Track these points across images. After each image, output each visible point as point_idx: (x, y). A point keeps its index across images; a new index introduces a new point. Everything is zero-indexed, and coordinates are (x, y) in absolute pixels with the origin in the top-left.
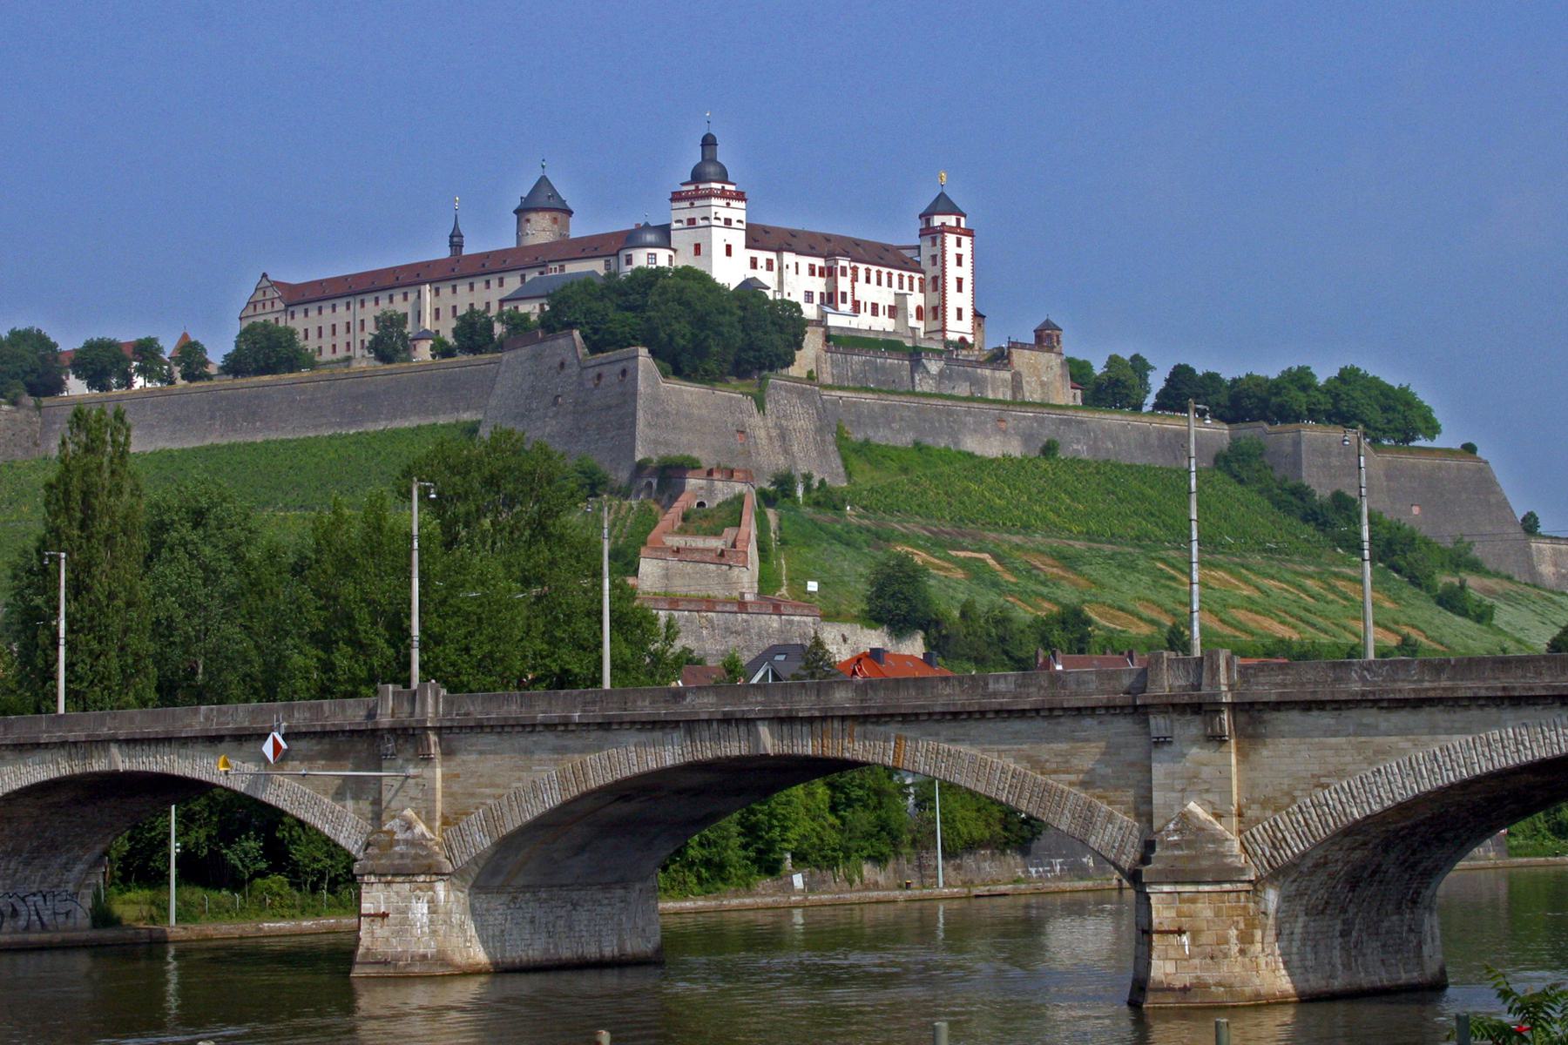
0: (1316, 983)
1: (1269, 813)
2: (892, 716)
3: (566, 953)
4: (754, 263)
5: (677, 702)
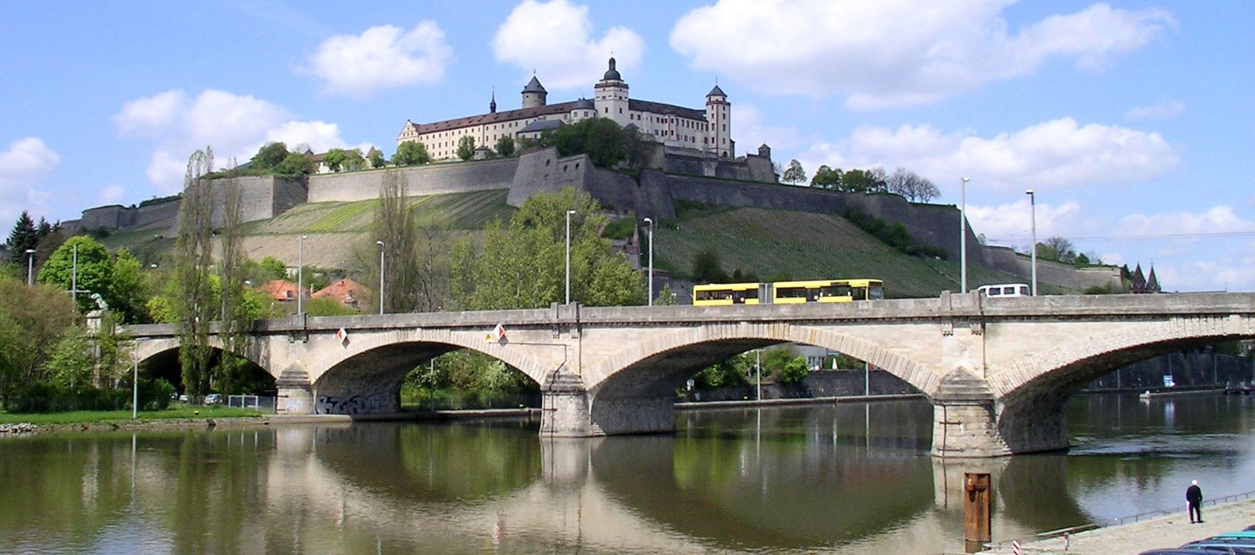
0: (1018, 448)
1: (1001, 368)
2: (809, 320)
3: (635, 429)
4: (632, 115)
5: (700, 313)
